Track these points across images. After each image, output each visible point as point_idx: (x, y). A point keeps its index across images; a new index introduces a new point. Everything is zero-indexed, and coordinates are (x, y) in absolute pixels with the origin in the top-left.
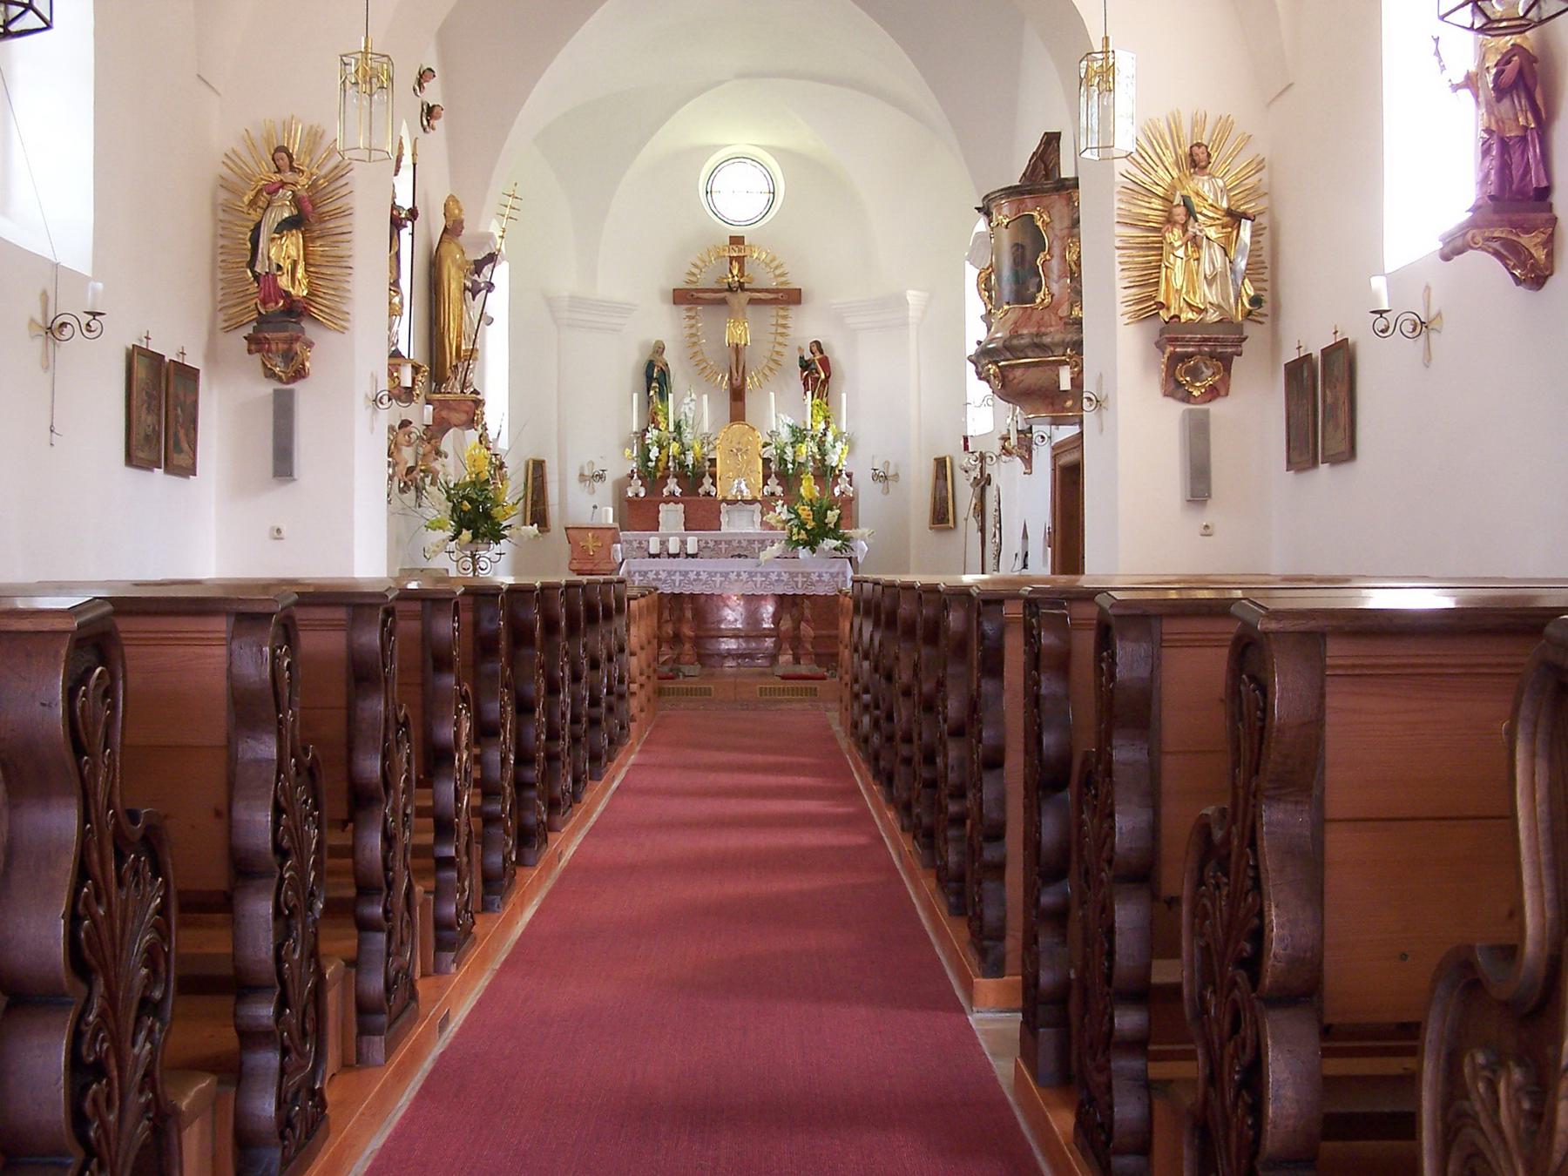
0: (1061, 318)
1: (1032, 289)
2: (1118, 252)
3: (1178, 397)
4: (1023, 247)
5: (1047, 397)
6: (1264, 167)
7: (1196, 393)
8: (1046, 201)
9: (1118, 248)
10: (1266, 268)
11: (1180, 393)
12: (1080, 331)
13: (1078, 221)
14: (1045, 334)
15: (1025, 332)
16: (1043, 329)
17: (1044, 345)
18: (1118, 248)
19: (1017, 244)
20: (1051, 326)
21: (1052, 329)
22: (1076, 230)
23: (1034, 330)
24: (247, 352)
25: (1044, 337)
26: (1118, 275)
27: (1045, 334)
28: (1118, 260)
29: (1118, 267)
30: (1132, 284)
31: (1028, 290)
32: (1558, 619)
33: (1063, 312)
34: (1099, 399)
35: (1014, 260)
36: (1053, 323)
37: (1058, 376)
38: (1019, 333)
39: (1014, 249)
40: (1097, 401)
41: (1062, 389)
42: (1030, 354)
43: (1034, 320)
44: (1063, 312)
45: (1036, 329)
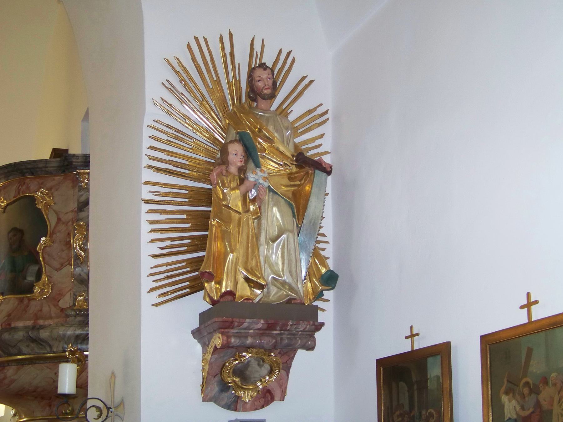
0: (62, 310)
1: (30, 278)
2: (146, 207)
3: (223, 403)
4: (21, 232)
5: (43, 398)
6: (328, 119)
7: (247, 399)
8: (50, 183)
9: (147, 202)
10: (327, 242)
11: (226, 397)
12: (85, 323)
13: (86, 203)
14: (42, 327)
15: (20, 324)
16: (41, 322)
17: (42, 340)
18: (147, 202)
19: (15, 230)
20: (51, 318)
21: (51, 322)
22: (82, 215)
23: (29, 323)
24: (309, 353)
25: (41, 331)
26: (146, 236)
27: (42, 327)
28: (146, 217)
29: (146, 227)
30: (164, 251)
31: (25, 278)
32: (79, 357)
33: (65, 302)
34: (109, 404)
35: (11, 245)
36: (53, 315)
37: (56, 374)
38: (13, 325)
39: (11, 234)
40: (108, 409)
41: (60, 391)
42: (24, 349)
43: (31, 312)
44: (65, 302)
45: (32, 322)
